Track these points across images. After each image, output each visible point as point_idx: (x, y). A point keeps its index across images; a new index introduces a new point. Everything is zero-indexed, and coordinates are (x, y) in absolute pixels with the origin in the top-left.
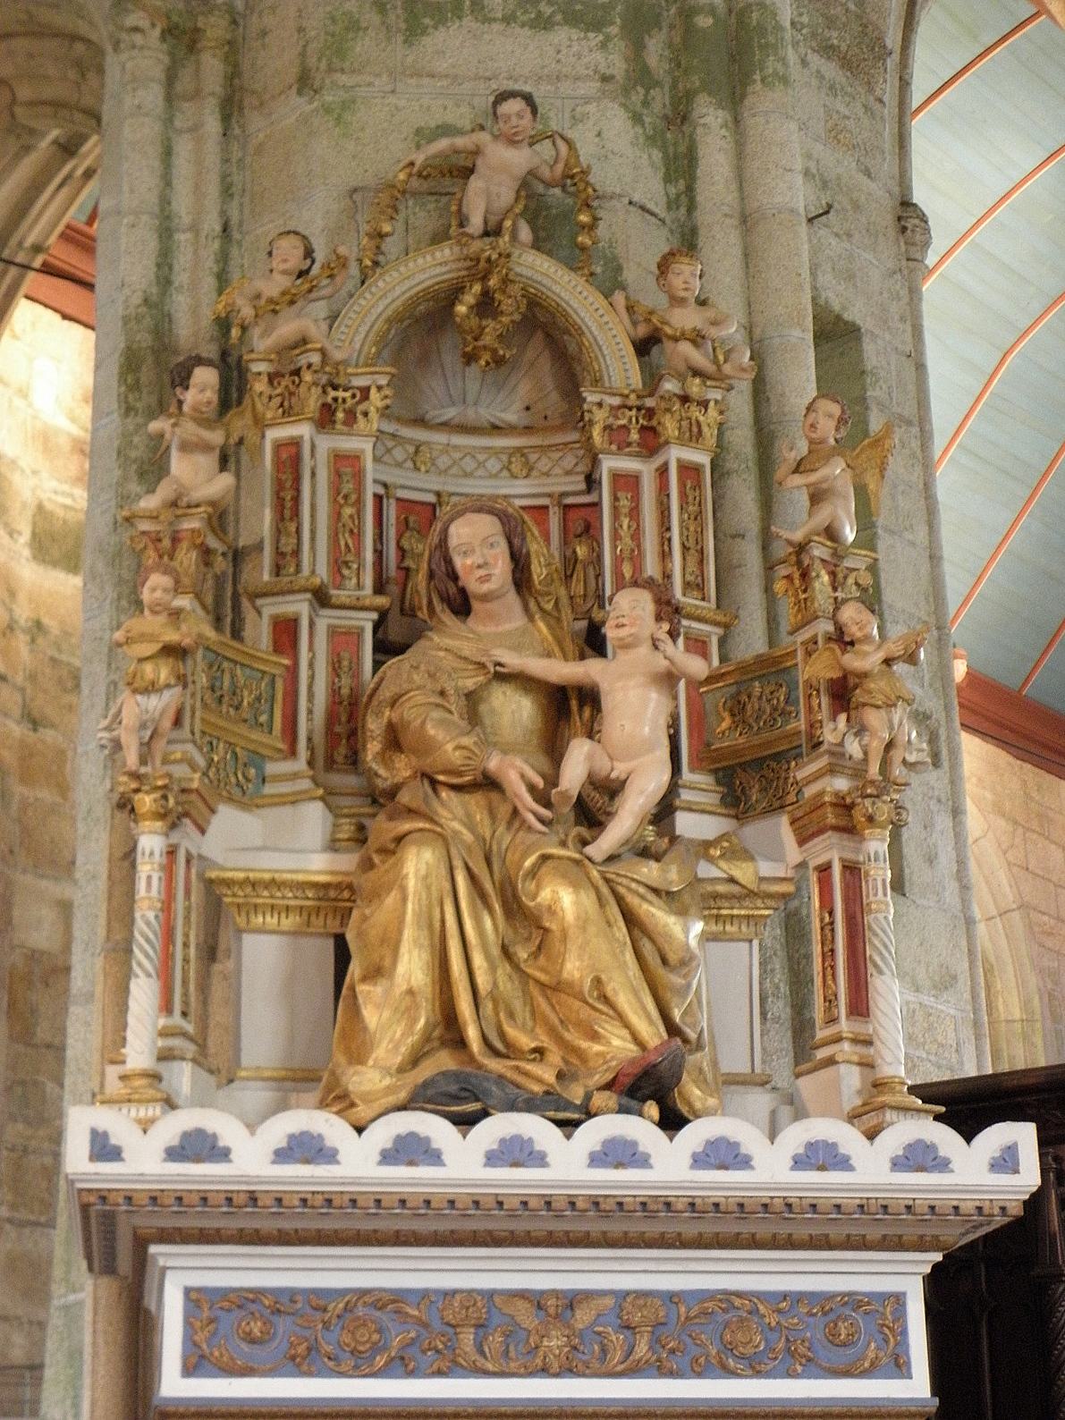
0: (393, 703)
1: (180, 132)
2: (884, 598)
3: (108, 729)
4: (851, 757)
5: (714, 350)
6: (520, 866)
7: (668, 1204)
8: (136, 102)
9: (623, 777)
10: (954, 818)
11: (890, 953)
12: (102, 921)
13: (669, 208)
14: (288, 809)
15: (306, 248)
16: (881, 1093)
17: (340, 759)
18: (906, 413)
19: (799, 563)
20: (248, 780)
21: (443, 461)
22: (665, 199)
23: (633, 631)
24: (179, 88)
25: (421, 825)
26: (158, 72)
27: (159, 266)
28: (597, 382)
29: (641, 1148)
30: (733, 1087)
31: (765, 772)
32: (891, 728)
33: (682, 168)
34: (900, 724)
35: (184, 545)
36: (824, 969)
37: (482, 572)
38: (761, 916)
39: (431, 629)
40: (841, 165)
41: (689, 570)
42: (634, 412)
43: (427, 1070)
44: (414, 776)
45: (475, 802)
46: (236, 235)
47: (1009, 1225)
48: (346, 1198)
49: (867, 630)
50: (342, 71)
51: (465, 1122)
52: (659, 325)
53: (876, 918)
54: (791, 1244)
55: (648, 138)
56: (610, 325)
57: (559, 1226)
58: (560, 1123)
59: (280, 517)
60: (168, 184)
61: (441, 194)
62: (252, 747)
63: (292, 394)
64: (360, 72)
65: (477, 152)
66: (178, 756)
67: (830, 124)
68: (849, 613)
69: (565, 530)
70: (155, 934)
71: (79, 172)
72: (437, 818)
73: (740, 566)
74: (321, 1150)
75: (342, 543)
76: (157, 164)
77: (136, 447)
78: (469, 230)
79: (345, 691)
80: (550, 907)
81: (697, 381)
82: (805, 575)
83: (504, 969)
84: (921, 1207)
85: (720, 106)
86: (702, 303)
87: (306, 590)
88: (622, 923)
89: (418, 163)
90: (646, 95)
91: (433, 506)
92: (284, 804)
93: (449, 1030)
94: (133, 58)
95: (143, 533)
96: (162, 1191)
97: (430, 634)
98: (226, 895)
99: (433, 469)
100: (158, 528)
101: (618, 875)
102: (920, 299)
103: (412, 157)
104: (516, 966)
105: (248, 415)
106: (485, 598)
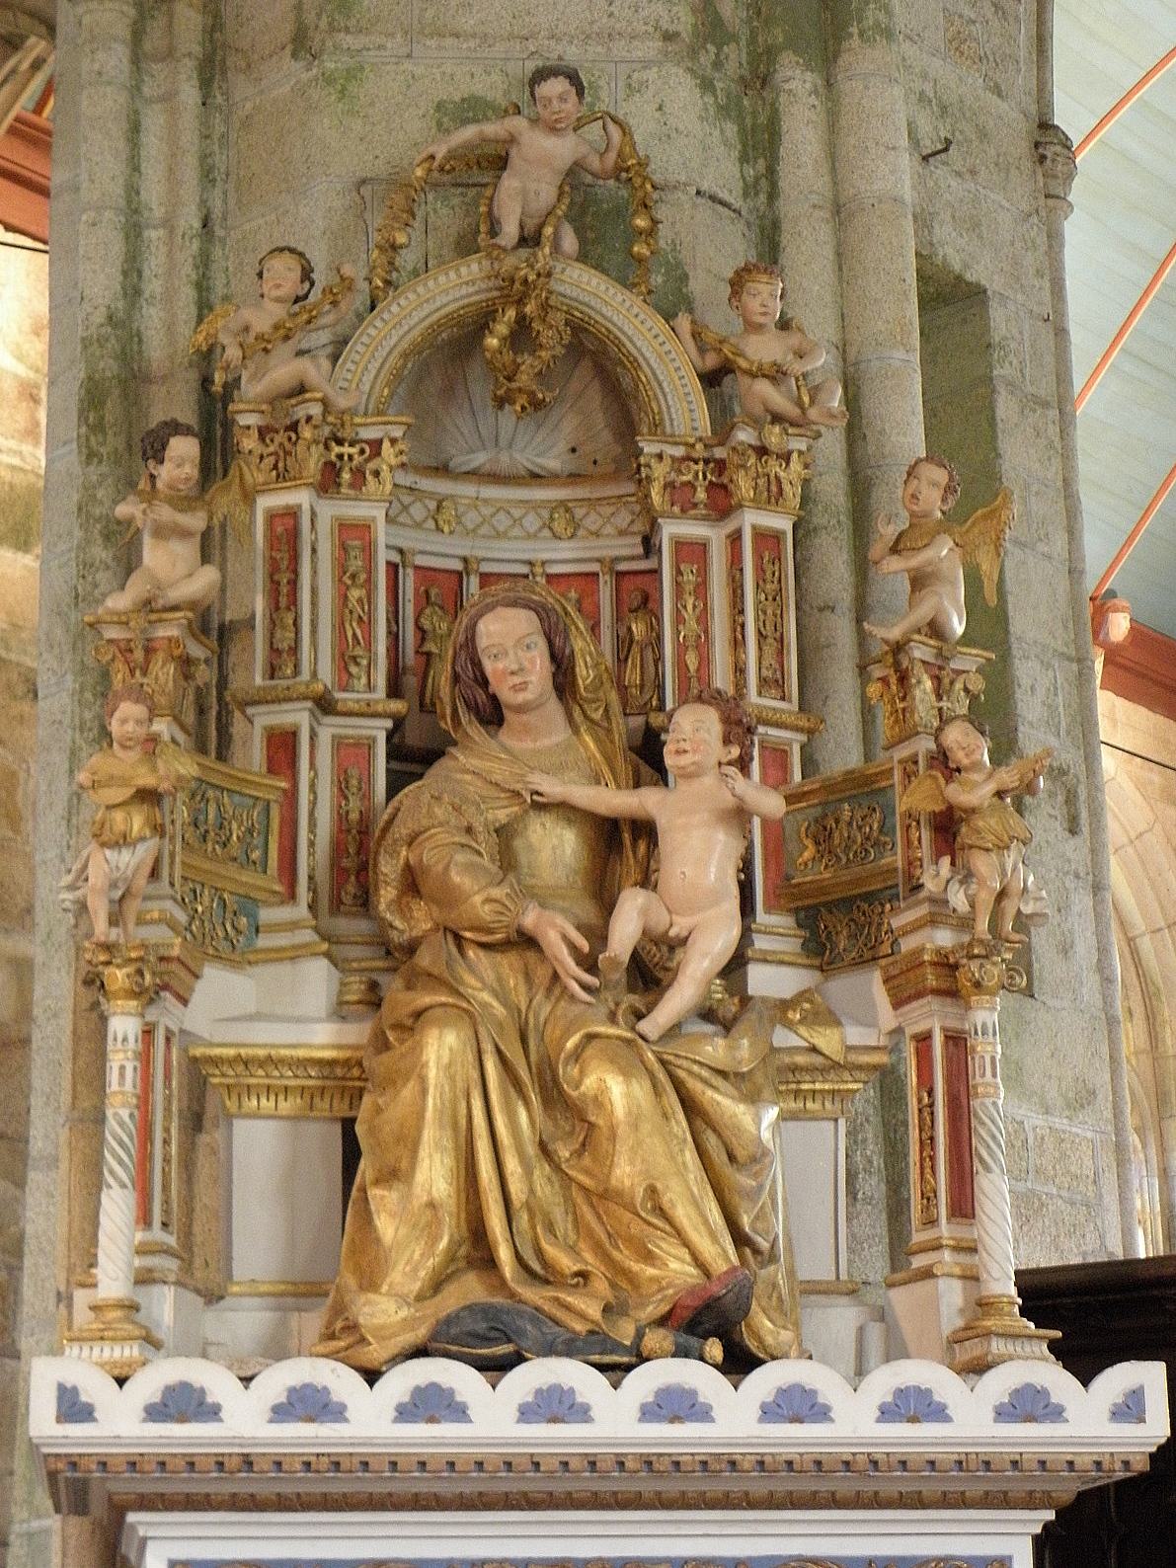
0: (410, 842)
1: (149, 101)
2: (1012, 629)
3: (72, 887)
4: (954, 910)
5: (798, 388)
6: (562, 1049)
7: (733, 1464)
8: (96, 66)
9: (684, 933)
10: (1095, 895)
11: (1000, 1146)
12: (67, 1084)
13: (745, 195)
14: (285, 969)
15: (303, 269)
16: (987, 1315)
17: (347, 899)
18: (1042, 393)
19: (897, 665)
20: (238, 932)
21: (471, 519)
22: (741, 184)
23: (697, 758)
24: (147, 46)
25: (443, 999)
26: (123, 30)
27: (125, 273)
28: (656, 427)
29: (701, 1399)
30: (813, 1298)
31: (856, 914)
32: (1003, 873)
33: (761, 143)
34: (1015, 869)
35: (160, 656)
36: (922, 1160)
37: (517, 680)
38: (848, 1090)
39: (455, 744)
40: (962, 83)
41: (765, 663)
42: (701, 466)
43: (452, 1300)
44: (436, 928)
45: (508, 965)
46: (219, 232)
47: (1130, 1479)
48: (356, 1460)
49: (976, 757)
50: (347, 30)
51: (495, 1368)
52: (730, 355)
53: (983, 1104)
54: (877, 1502)
55: (720, 107)
56: (673, 355)
57: (604, 1487)
58: (602, 1368)
59: (274, 607)
60: (136, 168)
61: (468, 186)
62: (241, 891)
63: (287, 453)
64: (368, 32)
65: (512, 139)
66: (156, 915)
67: (949, 35)
68: (957, 736)
69: (618, 601)
70: (131, 1138)
71: (25, 66)
72: (461, 989)
73: (828, 646)
74: (326, 1406)
75: (350, 634)
76: (121, 145)
77: (101, 503)
78: (502, 241)
79: (354, 816)
80: (596, 1097)
81: (777, 429)
82: (903, 678)
83: (542, 1171)
84: (1030, 1464)
85: (808, 67)
86: (784, 325)
87: (306, 698)
88: (681, 1116)
89: (439, 156)
90: (717, 55)
91: (460, 574)
92: (281, 960)
93: (476, 1249)
94: (90, 11)
95: (110, 641)
96: (141, 1455)
97: (452, 750)
98: (214, 1076)
99: (459, 528)
100: (128, 636)
101: (677, 1056)
102: (1062, 245)
103: (431, 150)
104: (557, 1168)
105: (236, 487)
106: (520, 709)
